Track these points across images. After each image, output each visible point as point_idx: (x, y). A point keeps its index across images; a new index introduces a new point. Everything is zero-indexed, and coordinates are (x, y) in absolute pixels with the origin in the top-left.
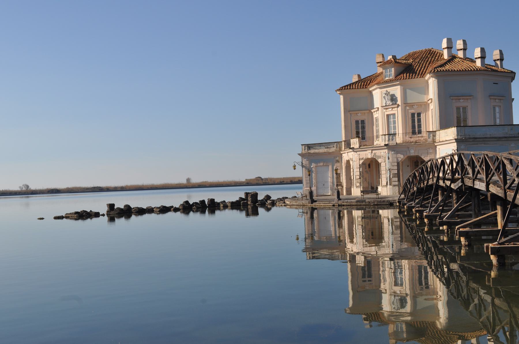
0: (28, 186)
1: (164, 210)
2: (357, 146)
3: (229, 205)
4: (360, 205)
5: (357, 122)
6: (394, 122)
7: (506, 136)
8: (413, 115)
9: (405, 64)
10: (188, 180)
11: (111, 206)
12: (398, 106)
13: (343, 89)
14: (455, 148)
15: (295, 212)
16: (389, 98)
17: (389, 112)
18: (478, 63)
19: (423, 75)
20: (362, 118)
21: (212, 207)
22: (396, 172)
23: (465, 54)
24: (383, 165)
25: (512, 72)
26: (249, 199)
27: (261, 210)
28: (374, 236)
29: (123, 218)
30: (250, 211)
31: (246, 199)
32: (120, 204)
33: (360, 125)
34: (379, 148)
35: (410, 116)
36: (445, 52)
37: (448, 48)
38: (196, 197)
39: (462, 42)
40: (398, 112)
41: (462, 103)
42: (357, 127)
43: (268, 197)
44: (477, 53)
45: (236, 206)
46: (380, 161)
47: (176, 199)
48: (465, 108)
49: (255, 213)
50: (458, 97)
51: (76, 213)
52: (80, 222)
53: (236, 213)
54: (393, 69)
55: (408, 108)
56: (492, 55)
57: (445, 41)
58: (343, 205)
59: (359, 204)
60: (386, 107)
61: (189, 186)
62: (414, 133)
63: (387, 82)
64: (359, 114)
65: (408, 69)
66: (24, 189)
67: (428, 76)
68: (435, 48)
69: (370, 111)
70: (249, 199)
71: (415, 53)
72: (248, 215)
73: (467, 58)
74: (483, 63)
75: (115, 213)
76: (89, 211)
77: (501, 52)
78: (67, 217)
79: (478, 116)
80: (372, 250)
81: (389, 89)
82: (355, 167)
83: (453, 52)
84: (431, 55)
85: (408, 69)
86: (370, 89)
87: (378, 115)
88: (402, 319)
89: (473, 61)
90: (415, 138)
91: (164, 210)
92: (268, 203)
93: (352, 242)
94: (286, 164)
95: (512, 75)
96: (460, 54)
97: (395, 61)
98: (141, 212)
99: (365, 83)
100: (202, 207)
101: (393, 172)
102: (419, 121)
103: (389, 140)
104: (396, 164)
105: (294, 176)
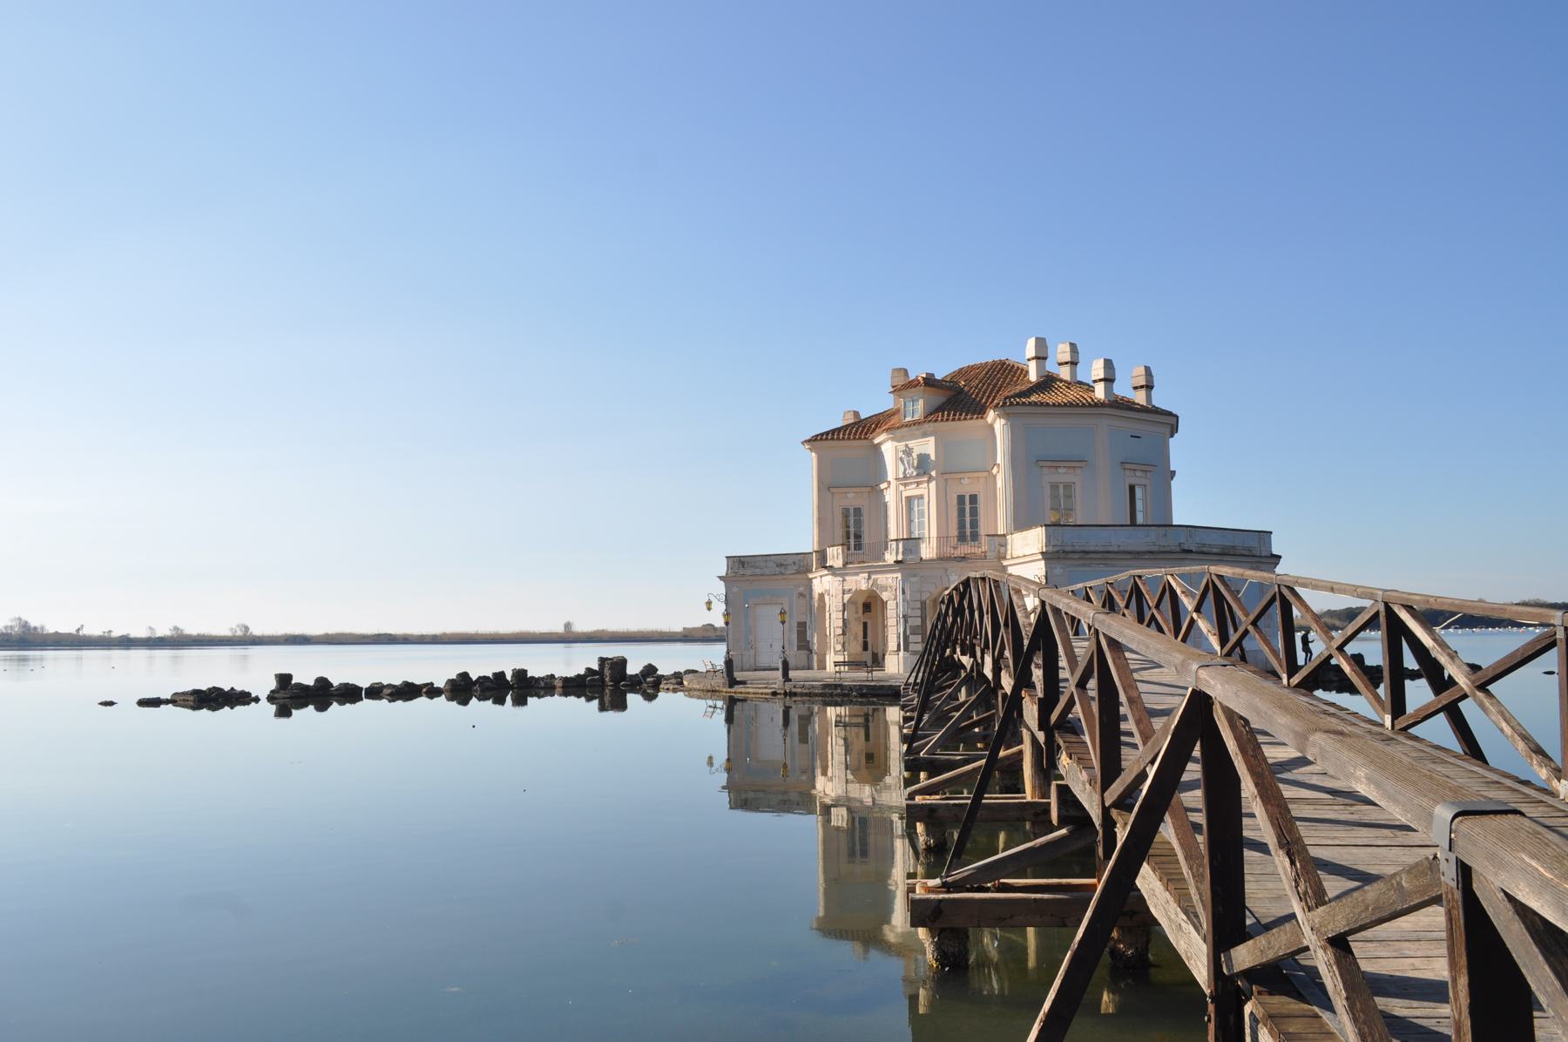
0: (247, 628)
1: (408, 692)
2: (838, 563)
3: (558, 684)
4: (831, 695)
5: (961, 499)
6: (921, 514)
7: (1152, 548)
10: (568, 625)
11: (284, 680)
13: (816, 441)
14: (1043, 572)
15: (701, 705)
17: (912, 491)
19: (981, 411)
20: (1069, 478)
21: (522, 687)
22: (918, 622)
23: (1073, 373)
24: (891, 605)
25: (1170, 414)
26: (607, 672)
27: (633, 699)
28: (870, 764)
29: (311, 707)
30: (607, 699)
31: (600, 672)
32: (305, 676)
33: (852, 519)
34: (887, 569)
35: (955, 502)
37: (1037, 358)
38: (482, 663)
39: (1068, 348)
40: (928, 491)
41: (1062, 476)
42: (961, 512)
43: (650, 670)
44: (1098, 371)
45: (575, 686)
46: (885, 596)
47: (439, 667)
48: (1068, 487)
49: (621, 705)
50: (1055, 462)
51: (196, 692)
52: (204, 713)
53: (576, 703)
54: (921, 402)
57: (1031, 343)
58: (795, 694)
59: (834, 693)
60: (904, 480)
61: (569, 638)
62: (962, 538)
64: (966, 481)
66: (239, 633)
67: (991, 415)
68: (1014, 358)
69: (989, 472)
70: (607, 672)
71: (971, 368)
72: (602, 708)
73: (1080, 383)
74: (1108, 391)
75: (290, 696)
76: (227, 689)
78: (174, 701)
79: (1098, 503)
80: (864, 793)
82: (833, 608)
83: (1051, 367)
84: (1002, 373)
85: (956, 398)
86: (876, 441)
87: (891, 497)
88: (1032, 962)
89: (1090, 389)
90: (965, 549)
91: (408, 692)
92: (650, 683)
93: (824, 773)
94: (697, 599)
95: (1170, 422)
97: (929, 381)
98: (350, 694)
99: (861, 429)
100: (496, 688)
101: (911, 622)
102: (974, 512)
105: (600, 628)
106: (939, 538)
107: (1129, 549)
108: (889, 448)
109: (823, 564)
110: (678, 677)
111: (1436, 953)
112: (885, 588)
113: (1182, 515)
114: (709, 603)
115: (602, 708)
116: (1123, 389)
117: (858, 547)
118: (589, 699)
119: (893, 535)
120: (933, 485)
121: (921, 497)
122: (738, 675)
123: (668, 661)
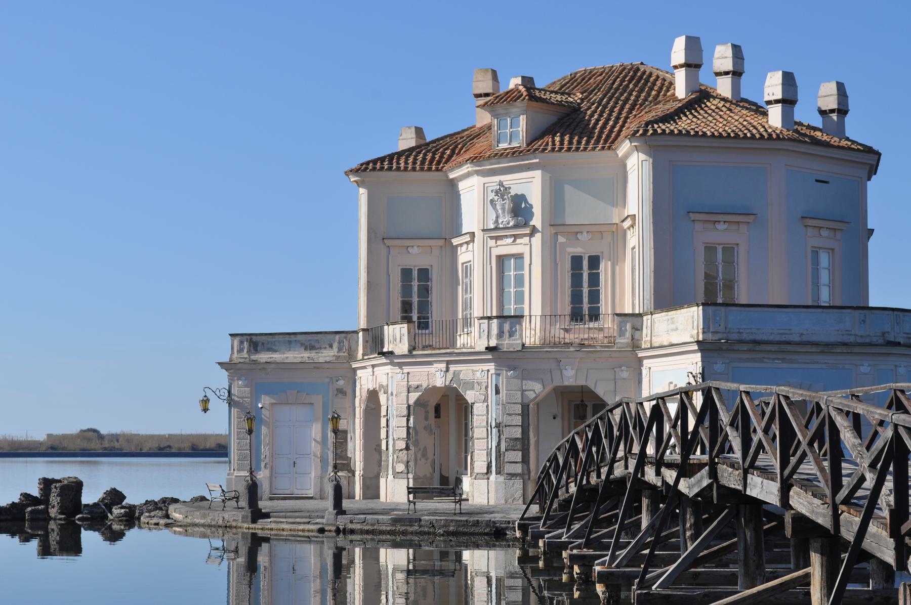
2: (402, 348)
5: (406, 274)
6: (519, 281)
8: (576, 261)
9: (560, 104)
12: (534, 231)
15: (200, 546)
16: (508, 204)
17: (506, 247)
18: (775, 117)
19: (610, 142)
22: (518, 433)
23: (736, 88)
25: (869, 150)
26: (54, 499)
27: (90, 538)
30: (54, 538)
31: (44, 499)
33: (415, 284)
34: (471, 357)
35: (568, 265)
36: (680, 80)
37: (687, 65)
40: (532, 250)
41: (721, 234)
43: (115, 497)
44: (773, 87)
46: (470, 396)
48: (729, 250)
49: (72, 546)
50: (714, 214)
54: (523, 120)
55: (561, 239)
56: (816, 96)
57: (680, 44)
58: (352, 532)
59: (402, 530)
60: (495, 233)
62: (576, 316)
63: (502, 155)
65: (568, 120)
67: (625, 147)
68: (651, 65)
70: (54, 499)
71: (591, 74)
72: (45, 551)
74: (787, 116)
77: (841, 87)
79: (769, 276)
81: (506, 179)
82: (393, 412)
83: (704, 78)
85: (568, 120)
86: (452, 176)
90: (581, 332)
92: (114, 517)
94: (184, 394)
95: (868, 159)
96: (724, 87)
99: (435, 155)
101: (508, 433)
102: (594, 280)
103: (500, 335)
104: (518, 409)
106: (543, 316)
107: (814, 338)
108: (474, 191)
109: (375, 343)
110: (162, 506)
111: (492, 495)
112: (470, 385)
113: (879, 296)
114: (205, 401)
115: (45, 551)
116: (806, 114)
117: (423, 324)
118: (26, 539)
119: (477, 312)
120: (537, 239)
121: (519, 257)
122: (264, 505)
123: (140, 483)
